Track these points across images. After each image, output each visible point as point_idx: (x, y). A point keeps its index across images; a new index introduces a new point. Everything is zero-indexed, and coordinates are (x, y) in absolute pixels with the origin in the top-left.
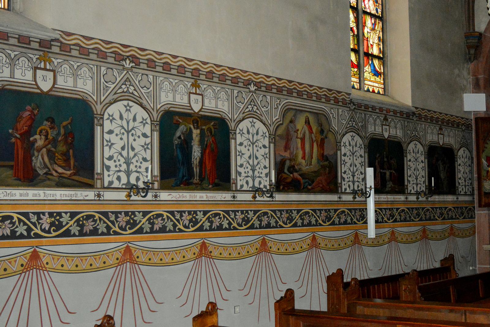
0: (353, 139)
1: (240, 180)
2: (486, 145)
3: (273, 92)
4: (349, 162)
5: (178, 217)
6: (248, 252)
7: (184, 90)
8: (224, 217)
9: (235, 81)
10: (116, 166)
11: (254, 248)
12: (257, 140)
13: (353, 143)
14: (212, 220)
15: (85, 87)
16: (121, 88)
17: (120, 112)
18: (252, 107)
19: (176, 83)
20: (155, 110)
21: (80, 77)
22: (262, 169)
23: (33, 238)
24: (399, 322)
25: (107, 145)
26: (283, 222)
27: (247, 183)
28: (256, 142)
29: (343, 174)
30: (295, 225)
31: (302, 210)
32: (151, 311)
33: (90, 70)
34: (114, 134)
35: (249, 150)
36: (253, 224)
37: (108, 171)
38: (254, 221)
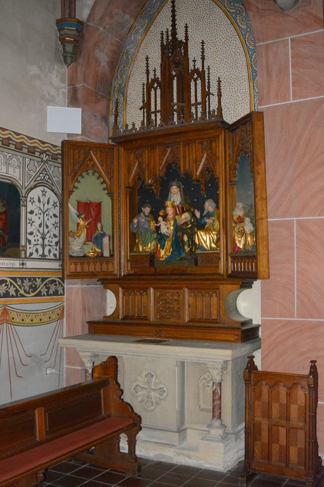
0: (44, 195)
1: (30, 248)
2: (76, 184)
3: (23, 151)
4: (37, 222)
5: (19, 283)
6: (41, 320)
7: (3, 159)
8: (59, 283)
9: (32, 151)
10: (35, 240)
11: (55, 314)
12: (48, 209)
13: (44, 199)
14: (49, 286)
15: (14, 174)
16: (39, 176)
17: (39, 197)
18: (44, 177)
19: (10, 157)
20: (24, 188)
21: (11, 166)
22: (52, 238)
23: (19, 297)
24: (48, 425)
25: (29, 223)
26: (25, 291)
27: (37, 251)
28: (47, 210)
29: (28, 234)
30: (39, 294)
31: (49, 278)
32: (25, 365)
33: (18, 160)
34: (34, 214)
35: (39, 218)
36: (40, 292)
37: (30, 244)
38: (42, 288)
